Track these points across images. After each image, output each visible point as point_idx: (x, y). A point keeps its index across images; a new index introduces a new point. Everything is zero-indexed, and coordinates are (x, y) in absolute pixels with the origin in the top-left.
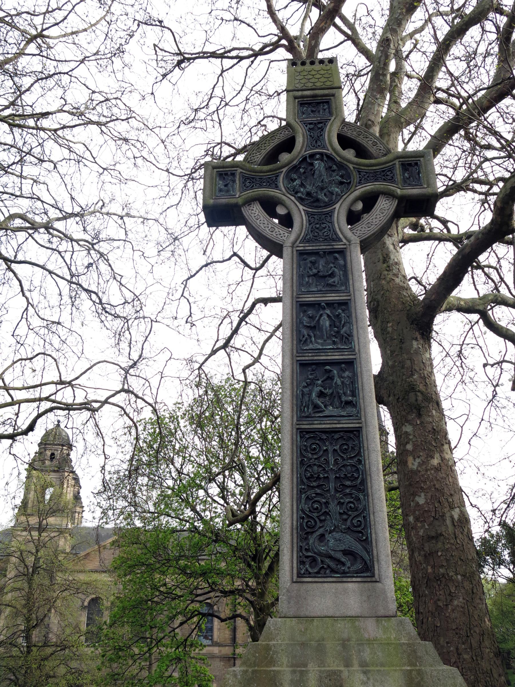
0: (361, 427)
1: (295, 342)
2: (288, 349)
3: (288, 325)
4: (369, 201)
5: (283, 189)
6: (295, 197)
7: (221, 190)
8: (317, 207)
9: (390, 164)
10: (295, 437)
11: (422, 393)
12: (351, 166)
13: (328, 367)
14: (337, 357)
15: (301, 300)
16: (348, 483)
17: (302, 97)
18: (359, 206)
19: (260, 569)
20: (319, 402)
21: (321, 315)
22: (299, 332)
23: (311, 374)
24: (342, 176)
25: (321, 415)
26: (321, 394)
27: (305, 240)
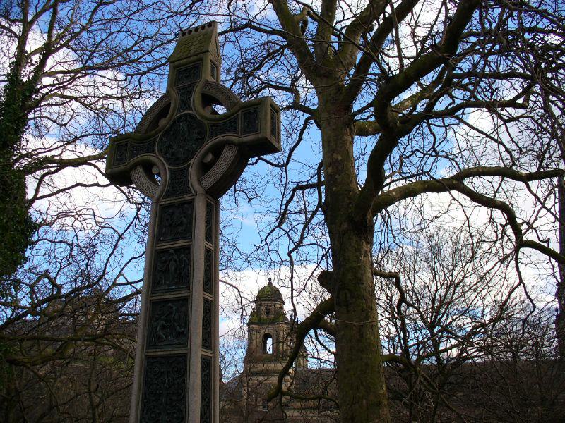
0: (186, 353)
1: (151, 285)
2: (148, 267)
3: (149, 251)
4: (217, 151)
5: (157, 152)
6: (163, 157)
7: (117, 160)
8: (177, 165)
9: (168, 171)
10: (144, 362)
11: (81, 97)
12: (206, 122)
13: (170, 304)
14: (176, 295)
15: (158, 248)
16: (174, 398)
17: (180, 66)
18: (210, 157)
19: (150, 131)
20: (162, 334)
21: (171, 260)
22: (154, 276)
23: (160, 311)
24: (199, 134)
25: (162, 344)
26: (163, 328)
27: (167, 195)
